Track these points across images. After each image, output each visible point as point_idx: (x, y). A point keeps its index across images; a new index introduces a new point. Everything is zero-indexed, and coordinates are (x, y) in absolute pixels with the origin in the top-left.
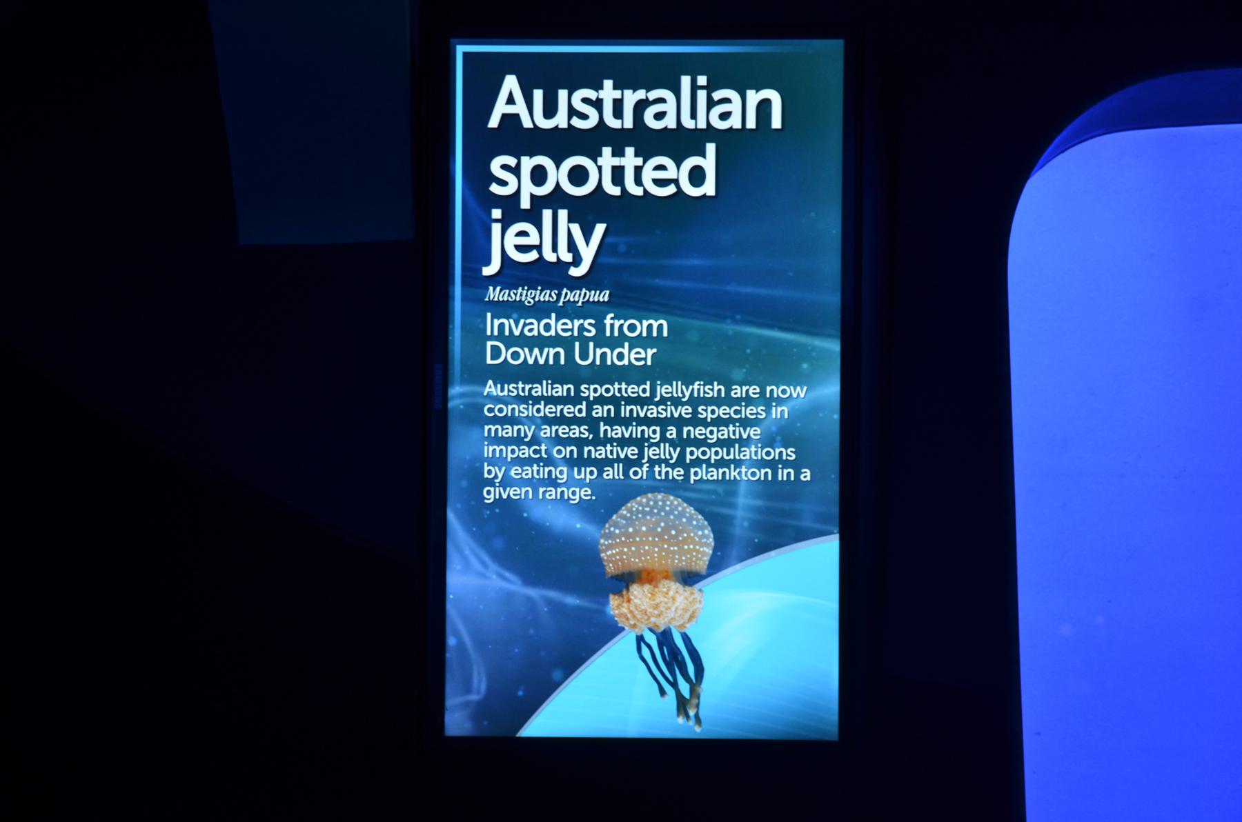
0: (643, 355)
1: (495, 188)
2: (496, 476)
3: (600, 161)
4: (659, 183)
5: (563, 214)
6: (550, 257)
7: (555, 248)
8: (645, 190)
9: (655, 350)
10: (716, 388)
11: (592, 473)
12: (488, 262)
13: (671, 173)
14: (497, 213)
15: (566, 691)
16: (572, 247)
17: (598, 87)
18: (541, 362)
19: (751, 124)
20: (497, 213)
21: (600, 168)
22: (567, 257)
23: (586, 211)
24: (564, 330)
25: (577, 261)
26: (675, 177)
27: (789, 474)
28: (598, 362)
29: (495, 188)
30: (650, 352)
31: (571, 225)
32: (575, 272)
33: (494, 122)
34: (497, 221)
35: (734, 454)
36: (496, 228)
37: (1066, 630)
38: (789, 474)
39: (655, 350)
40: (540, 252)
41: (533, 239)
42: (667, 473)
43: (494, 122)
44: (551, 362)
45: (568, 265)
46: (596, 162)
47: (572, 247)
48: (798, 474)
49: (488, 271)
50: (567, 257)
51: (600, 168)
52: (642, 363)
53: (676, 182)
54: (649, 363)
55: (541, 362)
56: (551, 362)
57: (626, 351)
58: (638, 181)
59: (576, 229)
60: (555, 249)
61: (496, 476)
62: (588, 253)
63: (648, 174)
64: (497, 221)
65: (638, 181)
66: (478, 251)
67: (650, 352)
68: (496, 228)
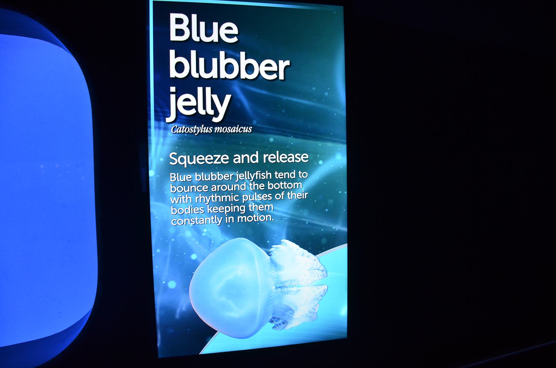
0: (274, 68)
5: (208, 89)
6: (202, 112)
7: (204, 108)
9: (287, 63)
10: (267, 174)
12: (169, 115)
14: (173, 89)
15: (211, 344)
16: (214, 107)
20: (173, 89)
22: (211, 112)
23: (219, 87)
24: (186, 108)
25: (216, 114)
26: (195, 105)
28: (195, 156)
30: (283, 64)
31: (213, 96)
32: (215, 120)
33: (257, 152)
34: (173, 93)
35: (221, 198)
36: (173, 97)
37: (158, 176)
39: (287, 63)
40: (197, 109)
41: (193, 103)
43: (257, 152)
45: (212, 116)
47: (214, 107)
49: (168, 120)
50: (211, 112)
52: (274, 76)
54: (281, 77)
59: (215, 97)
60: (204, 108)
62: (222, 110)
64: (173, 93)
65: (277, 176)
66: (163, 110)
67: (283, 64)
68: (173, 97)
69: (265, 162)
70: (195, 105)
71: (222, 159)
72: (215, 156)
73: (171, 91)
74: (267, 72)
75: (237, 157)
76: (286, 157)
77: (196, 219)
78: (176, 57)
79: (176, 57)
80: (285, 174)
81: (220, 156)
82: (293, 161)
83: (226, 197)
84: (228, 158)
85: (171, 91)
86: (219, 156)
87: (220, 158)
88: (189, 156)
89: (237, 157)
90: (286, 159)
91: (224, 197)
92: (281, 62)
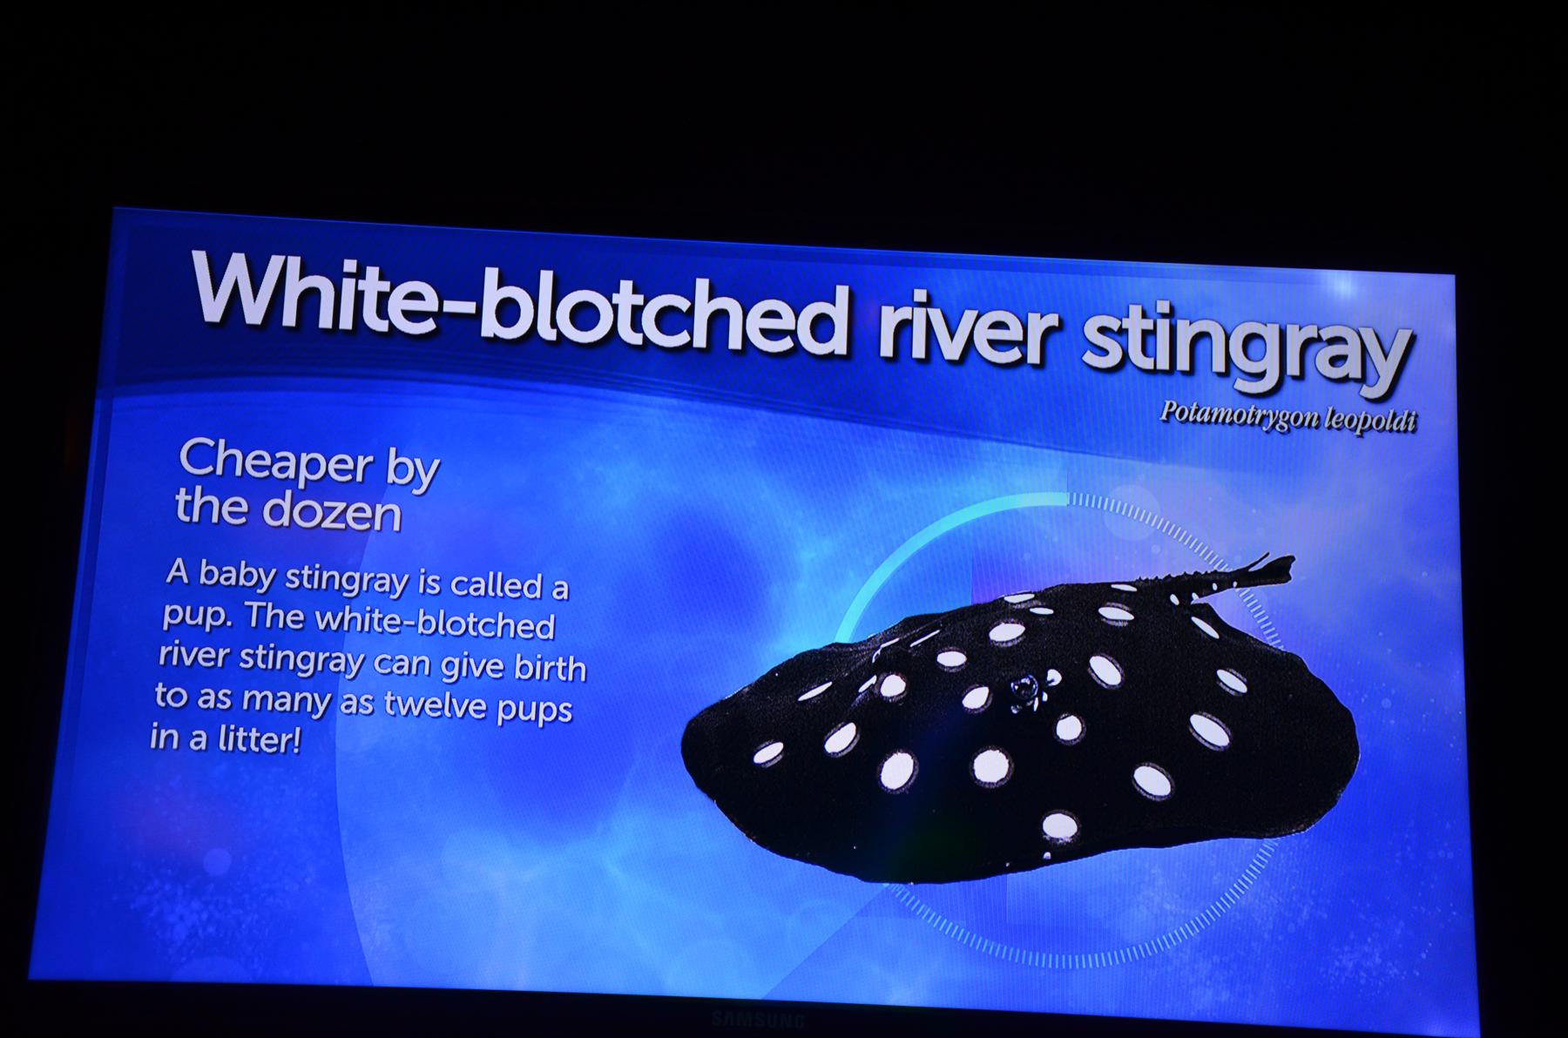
0: (1015, 333)
1: (1090, 358)
2: (259, 583)
3: (616, 298)
4: (411, 316)
8: (391, 325)
11: (216, 616)
13: (787, 322)
17: (609, 290)
18: (254, 313)
19: (1183, 363)
21: (615, 308)
26: (1020, 338)
27: (169, 737)
29: (1090, 358)
33: (842, 292)
38: (169, 737)
42: (207, 506)
43: (842, 292)
44: (289, 318)
46: (610, 300)
48: (185, 738)
51: (615, 308)
53: (793, 334)
55: (254, 313)
56: (289, 318)
57: (286, 505)
58: (382, 312)
61: (259, 583)
63: (397, 304)
65: (382, 312)
69: (887, 350)
70: (1020, 338)
71: (350, 515)
72: (327, 504)
73: (346, 269)
74: (994, 344)
75: (287, 459)
76: (268, 462)
77: (1135, 324)
78: (711, 297)
79: (711, 297)
80: (380, 510)
81: (341, 506)
82: (211, 704)
83: (259, 697)
84: (245, 508)
85: (346, 269)
86: (341, 506)
87: (345, 510)
88: (325, 321)
89: (287, 459)
90: (269, 468)
91: (254, 696)
92: (1033, 318)
